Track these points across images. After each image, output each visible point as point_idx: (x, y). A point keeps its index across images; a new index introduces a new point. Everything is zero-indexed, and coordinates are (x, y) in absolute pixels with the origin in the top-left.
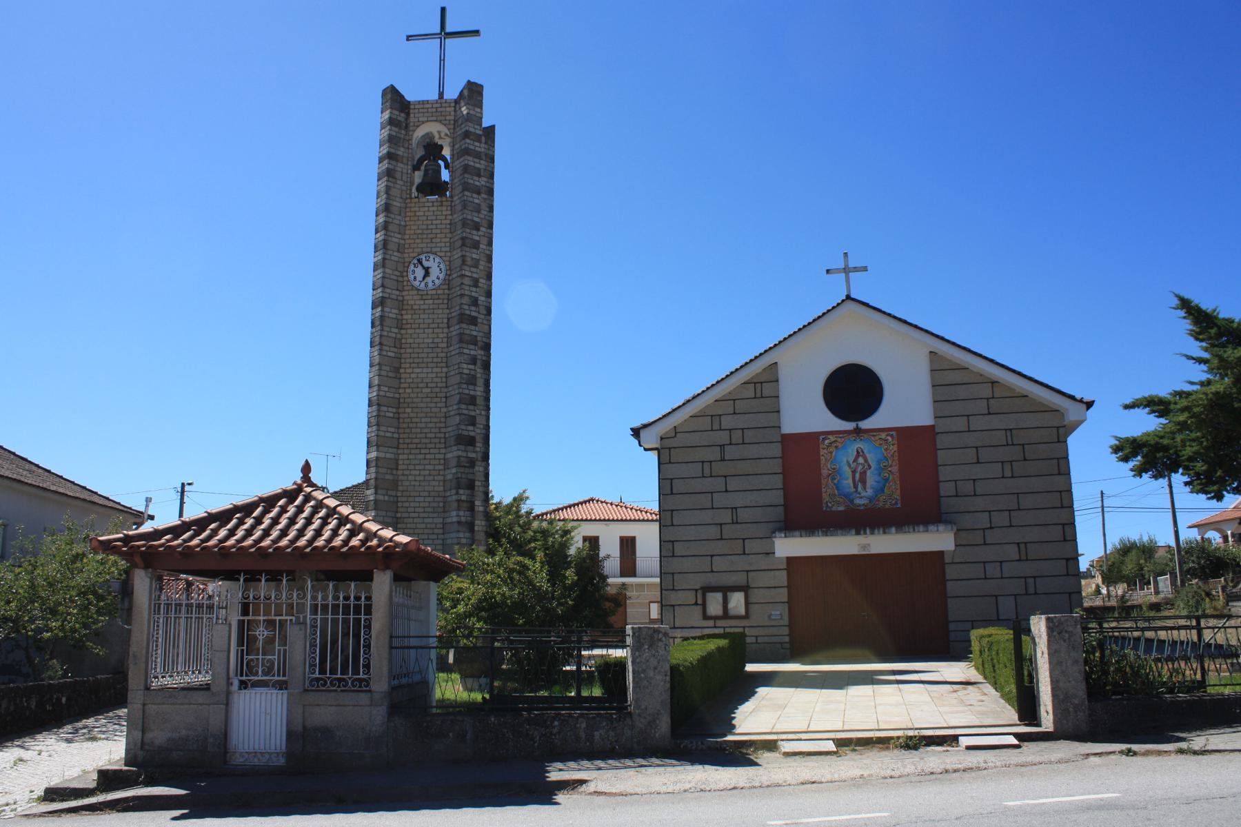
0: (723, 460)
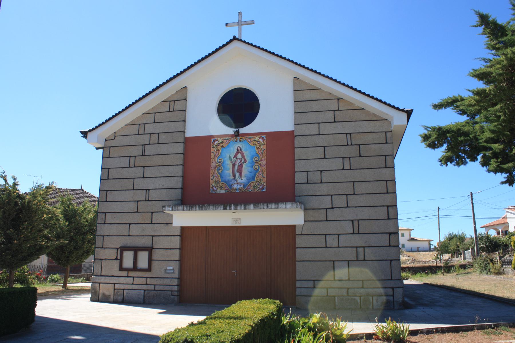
0: (143, 155)
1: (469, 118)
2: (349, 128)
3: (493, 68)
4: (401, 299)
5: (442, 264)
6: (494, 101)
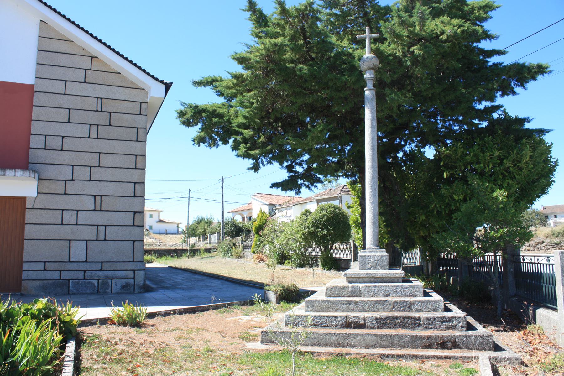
1: (226, 100)
2: (101, 92)
3: (253, 54)
4: (142, 282)
5: (188, 248)
6: (249, 87)
